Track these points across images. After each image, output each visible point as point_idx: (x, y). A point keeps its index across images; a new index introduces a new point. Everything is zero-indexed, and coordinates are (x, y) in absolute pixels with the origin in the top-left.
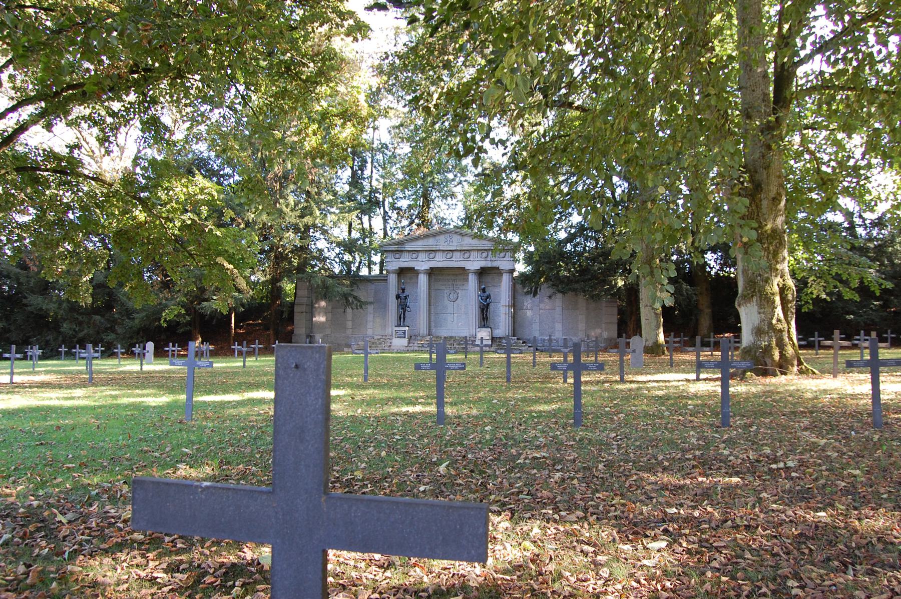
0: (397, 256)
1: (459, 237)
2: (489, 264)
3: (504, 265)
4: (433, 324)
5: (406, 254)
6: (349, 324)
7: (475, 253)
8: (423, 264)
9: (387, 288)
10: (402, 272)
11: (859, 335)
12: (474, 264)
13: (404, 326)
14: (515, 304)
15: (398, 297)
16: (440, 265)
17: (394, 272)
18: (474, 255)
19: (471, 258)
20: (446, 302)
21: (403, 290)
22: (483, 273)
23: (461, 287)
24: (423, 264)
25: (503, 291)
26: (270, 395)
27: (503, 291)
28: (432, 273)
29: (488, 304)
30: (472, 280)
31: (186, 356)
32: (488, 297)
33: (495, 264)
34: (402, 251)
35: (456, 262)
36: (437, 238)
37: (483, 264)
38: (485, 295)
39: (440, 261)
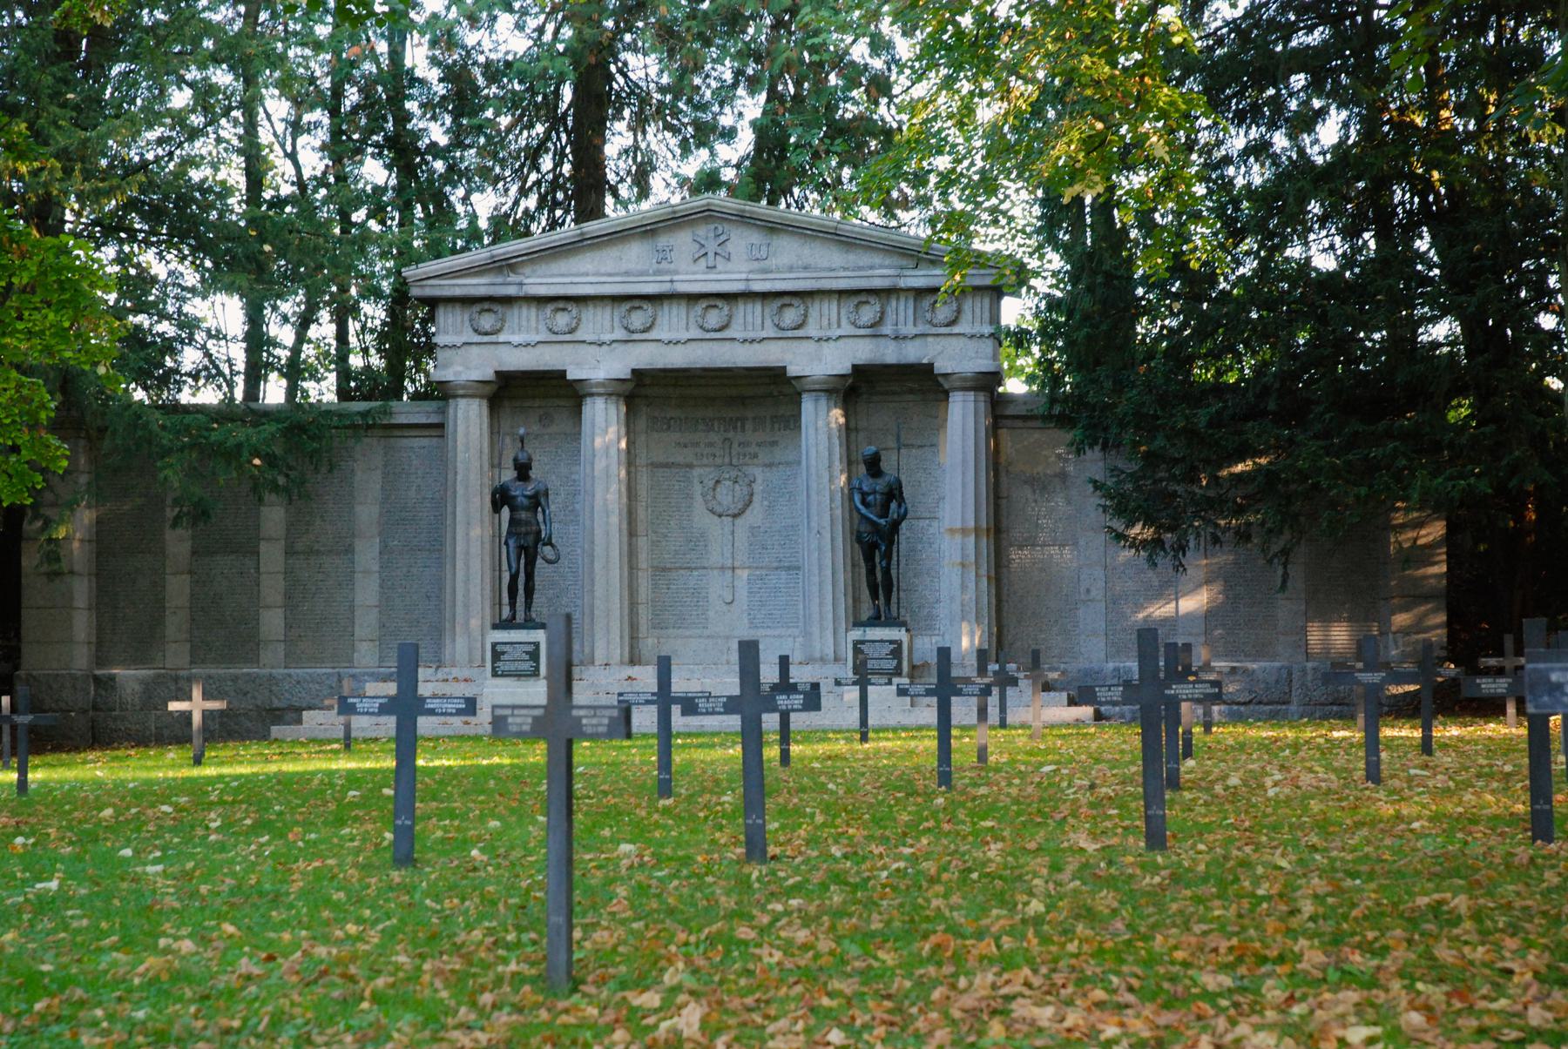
0: (487, 321)
1: (755, 237)
2: (890, 354)
3: (955, 355)
4: (644, 614)
5: (528, 314)
6: (272, 622)
7: (830, 308)
8: (599, 357)
9: (443, 463)
10: (512, 392)
11: (1500, 653)
12: (823, 352)
13: (529, 624)
14: (998, 527)
15: (501, 498)
16: (676, 358)
17: (477, 389)
18: (823, 316)
19: (812, 330)
20: (702, 518)
21: (523, 471)
22: (859, 388)
23: (764, 457)
24: (599, 357)
25: (949, 471)
26: (1444, 569)
27: (949, 471)
28: (644, 392)
29: (895, 526)
30: (823, 421)
31: (494, 707)
32: (895, 493)
33: (913, 353)
34: (508, 301)
35: (746, 345)
36: (663, 241)
37: (865, 352)
38: (881, 485)
39: (677, 344)
